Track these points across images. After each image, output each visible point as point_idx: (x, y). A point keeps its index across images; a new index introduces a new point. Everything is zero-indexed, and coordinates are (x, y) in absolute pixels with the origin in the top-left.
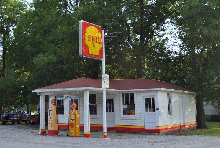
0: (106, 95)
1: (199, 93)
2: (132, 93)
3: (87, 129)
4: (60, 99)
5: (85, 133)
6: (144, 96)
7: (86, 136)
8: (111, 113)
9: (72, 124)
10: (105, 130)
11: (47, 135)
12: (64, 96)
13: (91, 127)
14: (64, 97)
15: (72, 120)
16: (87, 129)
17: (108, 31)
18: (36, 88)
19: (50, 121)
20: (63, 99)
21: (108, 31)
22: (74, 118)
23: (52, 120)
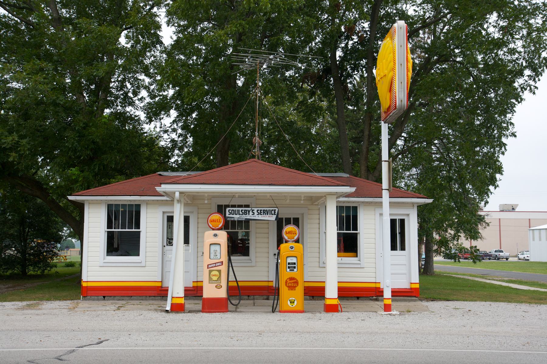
0: (218, 207)
1: (372, 101)
2: (351, 205)
3: (331, 293)
4: (238, 216)
5: (328, 302)
6: (164, 213)
7: (331, 309)
8: (398, 252)
9: (291, 279)
10: (387, 294)
11: (170, 313)
12: (256, 210)
13: (340, 289)
14: (255, 211)
15: (288, 270)
16: (331, 293)
17: (324, 37)
18: (429, 203)
19: (213, 273)
20: (249, 216)
21: (324, 37)
22: (295, 264)
23: (220, 271)
